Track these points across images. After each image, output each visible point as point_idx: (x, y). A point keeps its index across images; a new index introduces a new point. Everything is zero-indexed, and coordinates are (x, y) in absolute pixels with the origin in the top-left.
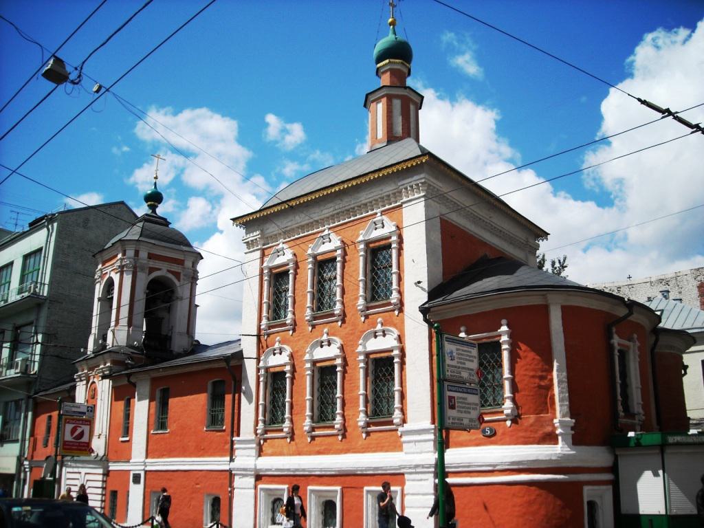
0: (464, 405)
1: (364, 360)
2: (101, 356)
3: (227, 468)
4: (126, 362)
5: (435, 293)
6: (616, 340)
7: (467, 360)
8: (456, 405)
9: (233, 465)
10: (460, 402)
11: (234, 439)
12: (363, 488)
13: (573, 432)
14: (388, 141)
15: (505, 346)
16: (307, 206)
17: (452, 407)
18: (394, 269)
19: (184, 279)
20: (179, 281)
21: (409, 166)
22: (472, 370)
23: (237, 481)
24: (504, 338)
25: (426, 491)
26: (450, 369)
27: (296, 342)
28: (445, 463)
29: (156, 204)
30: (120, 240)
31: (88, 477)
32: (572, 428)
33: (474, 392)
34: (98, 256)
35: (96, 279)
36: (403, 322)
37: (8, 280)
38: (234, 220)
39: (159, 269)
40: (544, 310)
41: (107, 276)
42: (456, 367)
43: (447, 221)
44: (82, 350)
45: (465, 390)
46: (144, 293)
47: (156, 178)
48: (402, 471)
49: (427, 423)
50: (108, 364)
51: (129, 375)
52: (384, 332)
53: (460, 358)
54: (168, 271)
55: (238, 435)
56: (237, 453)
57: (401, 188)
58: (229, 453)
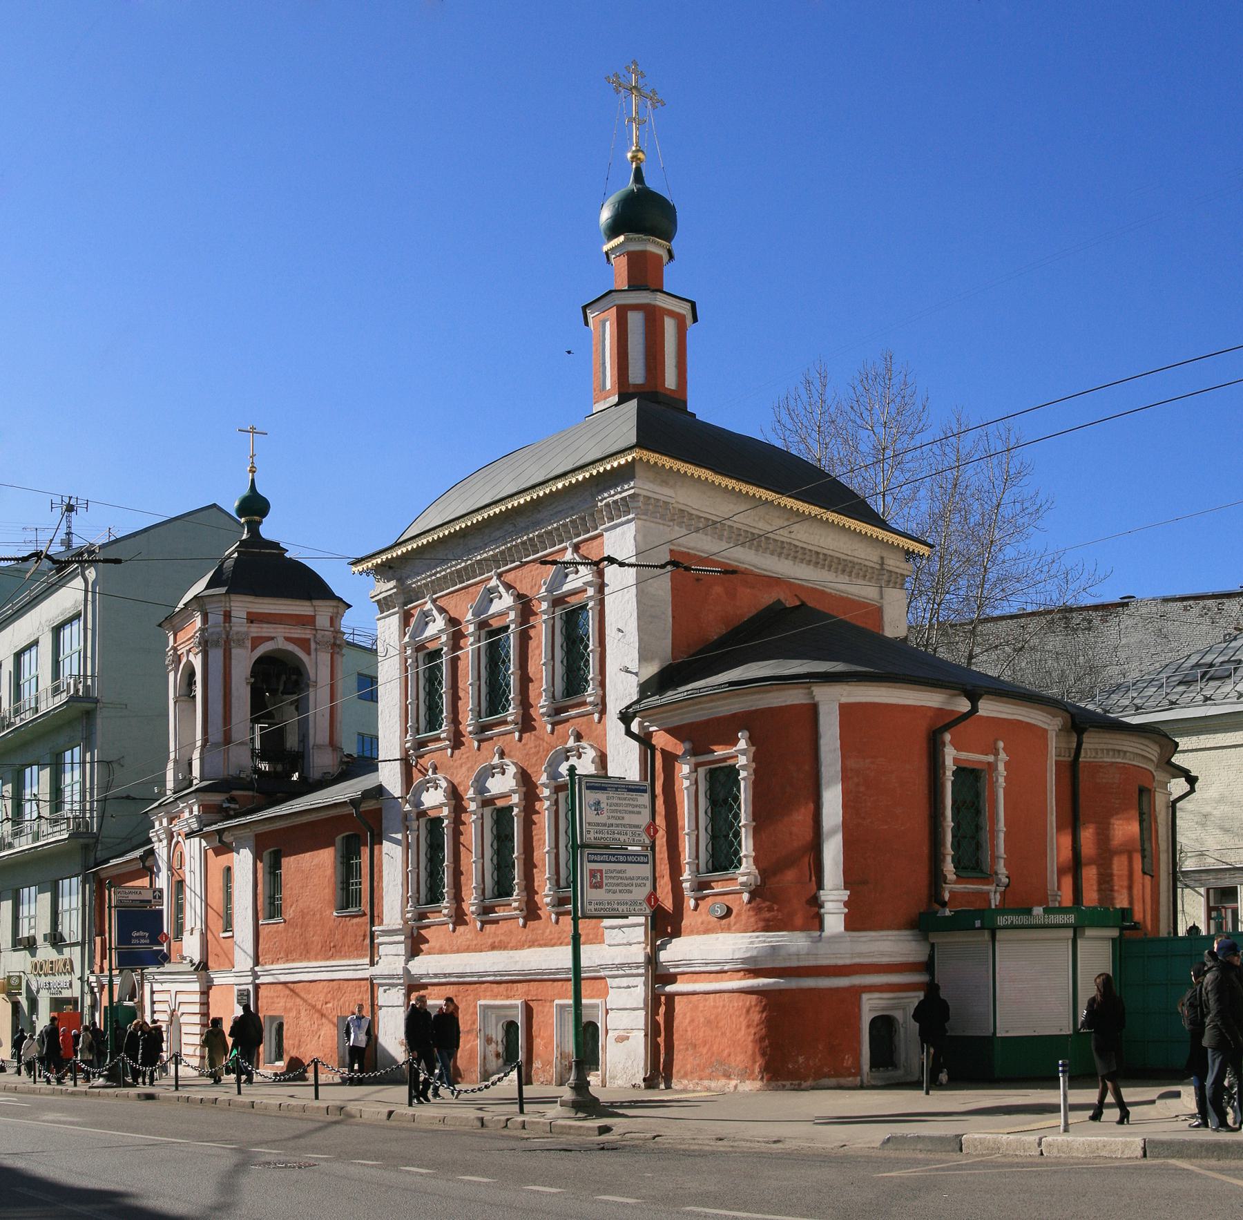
0: (620, 881)
3: (366, 974)
5: (646, 689)
7: (626, 812)
8: (605, 881)
10: (611, 877)
11: (374, 929)
15: (743, 774)
17: (598, 886)
20: (309, 654)
22: (637, 826)
23: (382, 997)
24: (742, 760)
26: (593, 829)
27: (457, 768)
28: (582, 965)
29: (257, 518)
30: (195, 597)
31: (181, 998)
33: (642, 859)
35: (168, 665)
37: (33, 672)
39: (272, 638)
42: (605, 825)
45: (621, 859)
48: (602, 974)
53: (613, 811)
54: (287, 639)
55: (381, 923)
56: (383, 950)
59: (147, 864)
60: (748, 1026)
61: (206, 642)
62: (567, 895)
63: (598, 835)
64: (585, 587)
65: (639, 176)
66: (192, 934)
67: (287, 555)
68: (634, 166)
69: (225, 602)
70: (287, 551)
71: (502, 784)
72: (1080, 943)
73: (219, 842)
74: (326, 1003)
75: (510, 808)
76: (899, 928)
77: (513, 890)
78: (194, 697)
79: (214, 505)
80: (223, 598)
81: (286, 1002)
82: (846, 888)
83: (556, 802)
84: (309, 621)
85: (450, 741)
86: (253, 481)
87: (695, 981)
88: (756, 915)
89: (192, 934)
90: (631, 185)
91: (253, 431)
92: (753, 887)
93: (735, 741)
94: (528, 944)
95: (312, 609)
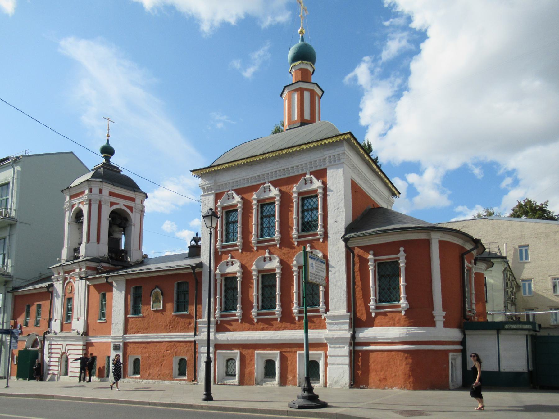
1: (280, 272)
2: (77, 264)
3: (192, 339)
4: (98, 268)
5: (349, 229)
6: (466, 263)
9: (196, 338)
11: (197, 320)
12: (296, 352)
13: (444, 320)
14: (301, 123)
15: (238, 279)
16: (251, 165)
18: (320, 211)
19: (135, 212)
21: (335, 141)
25: (343, 354)
28: (309, 338)
29: (109, 155)
31: (68, 347)
32: (444, 317)
34: (65, 192)
36: (326, 247)
38: (192, 171)
40: (427, 243)
41: (76, 207)
43: (354, 181)
44: (58, 259)
46: (108, 220)
47: (108, 136)
49: (343, 311)
50: (84, 269)
51: (107, 278)
52: (232, 262)
54: (125, 205)
57: (325, 156)
58: (194, 331)
59: (50, 289)
60: (407, 364)
61: (90, 200)
62: (302, 309)
63: (313, 278)
64: (275, 196)
65: (302, 40)
66: (78, 320)
67: (122, 173)
68: (301, 35)
69: (100, 185)
70: (122, 171)
71: (275, 264)
72: (500, 336)
73: (106, 281)
74: (167, 351)
75: (236, 278)
76: (455, 328)
77: (237, 309)
78: (82, 222)
79: (72, 153)
80: (99, 183)
81: (142, 350)
82: (443, 311)
83: (258, 277)
84: (133, 200)
85: (241, 246)
86: (108, 141)
87: (376, 346)
88: (409, 320)
89: (78, 320)
90: (300, 42)
91: (109, 119)
92: (406, 309)
93: (399, 252)
94: (282, 329)
95: (134, 195)
